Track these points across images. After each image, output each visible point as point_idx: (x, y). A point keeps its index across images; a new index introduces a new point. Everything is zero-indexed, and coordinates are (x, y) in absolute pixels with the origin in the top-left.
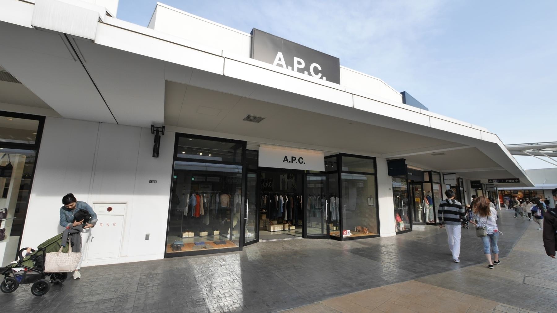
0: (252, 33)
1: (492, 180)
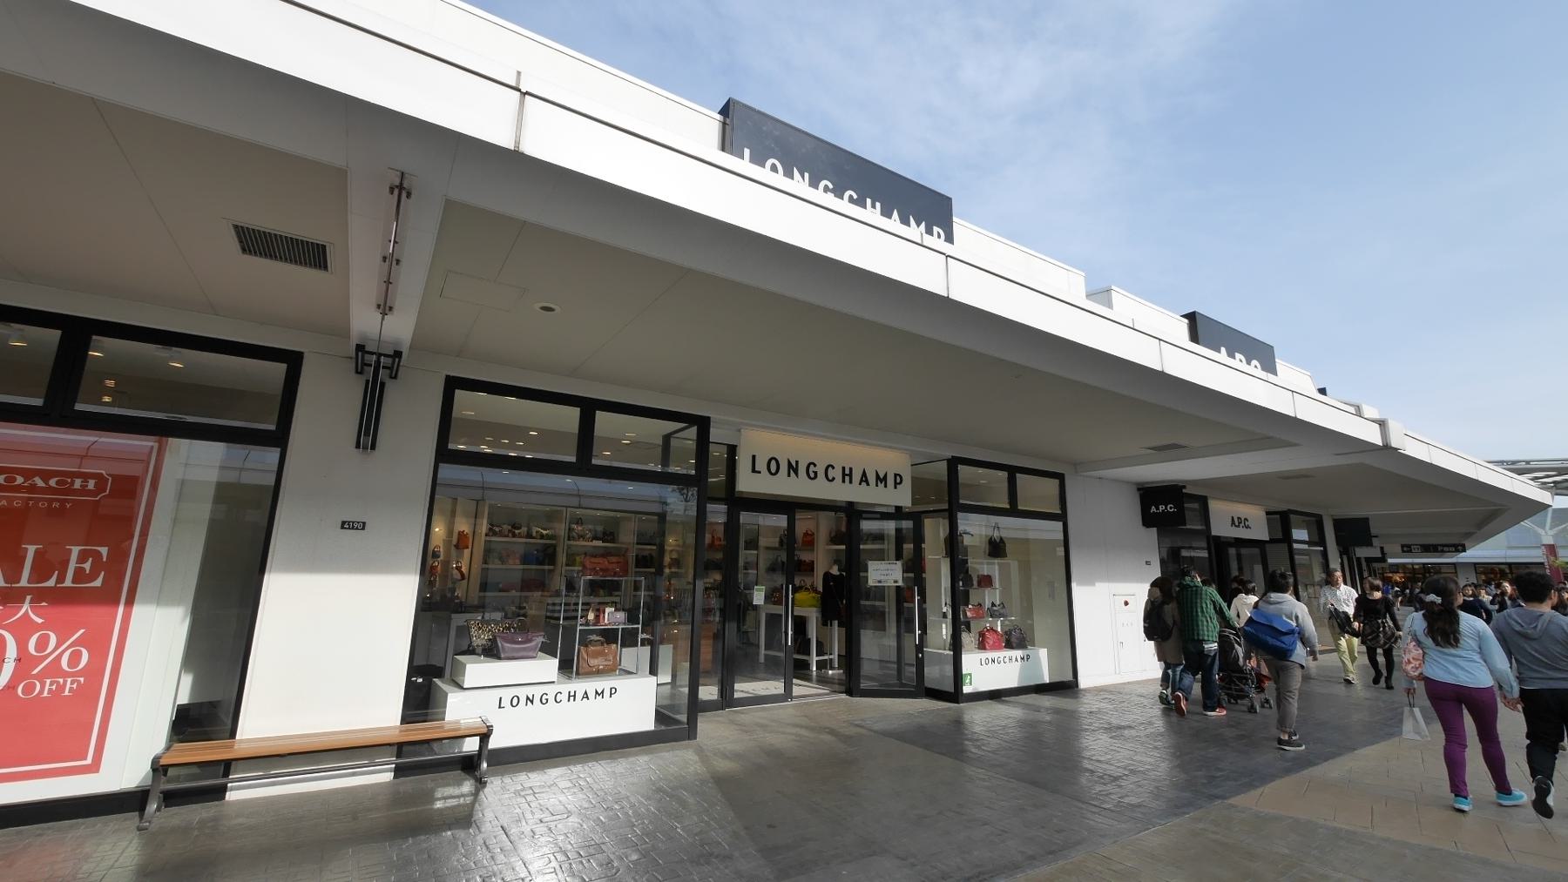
0: (725, 111)
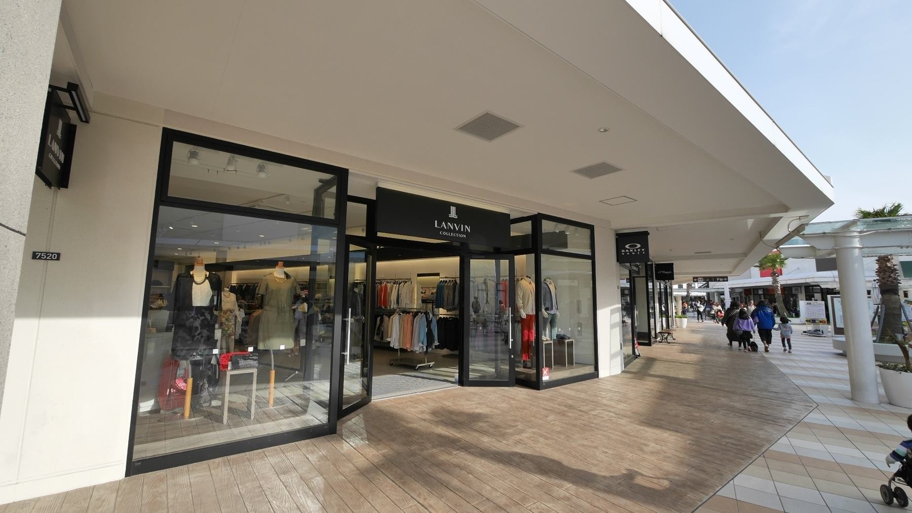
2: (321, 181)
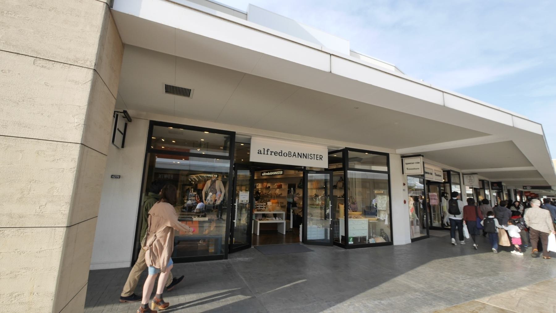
1: (526, 187)
2: (225, 137)
